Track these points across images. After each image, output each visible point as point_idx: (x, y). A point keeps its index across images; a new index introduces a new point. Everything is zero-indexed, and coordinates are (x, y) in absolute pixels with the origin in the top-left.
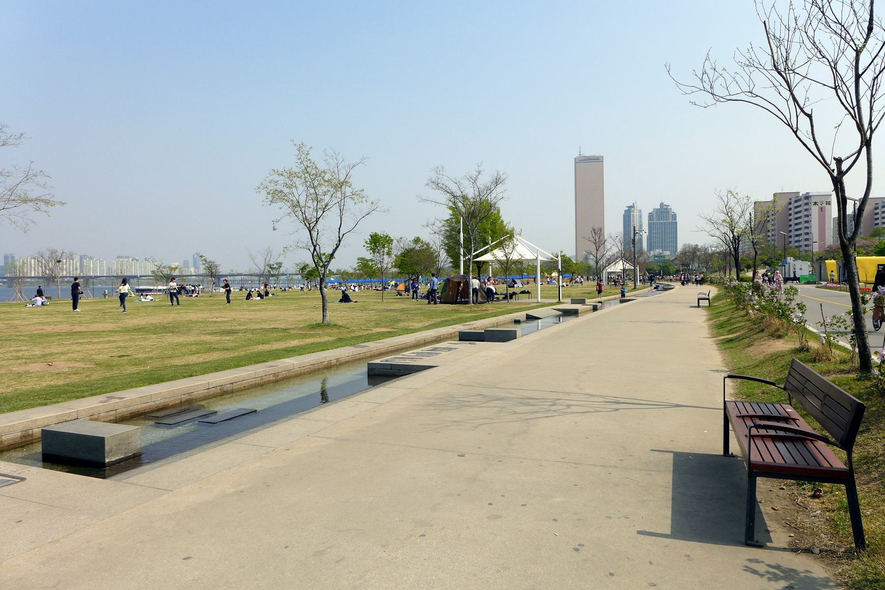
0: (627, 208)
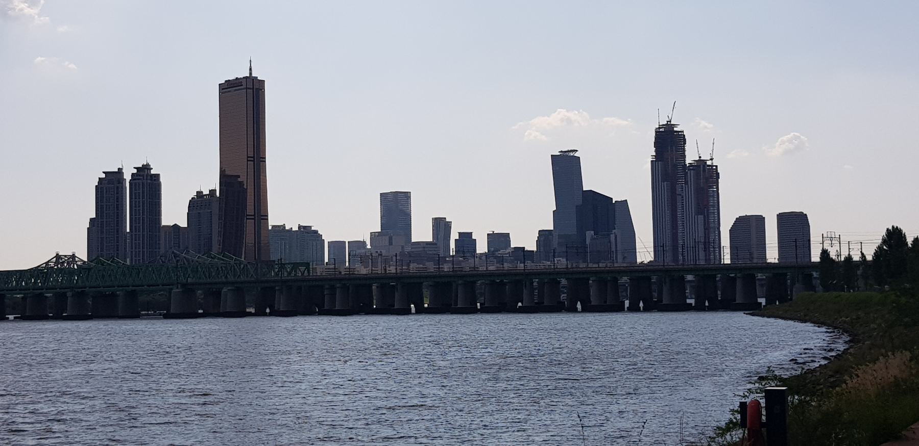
0: (103, 176)
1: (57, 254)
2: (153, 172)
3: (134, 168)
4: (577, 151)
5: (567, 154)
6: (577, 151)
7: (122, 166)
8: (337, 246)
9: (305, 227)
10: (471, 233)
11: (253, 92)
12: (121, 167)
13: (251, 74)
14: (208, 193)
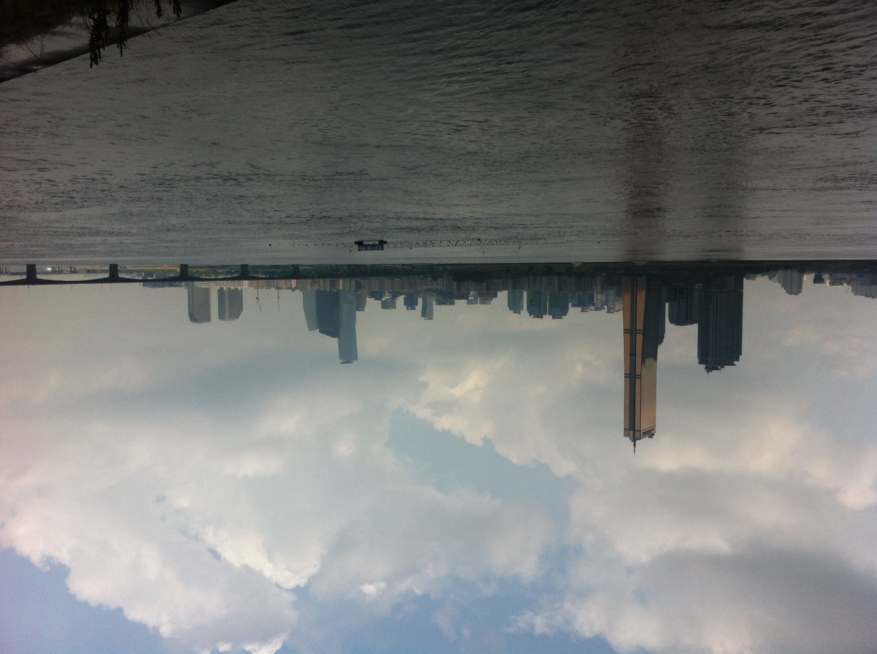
0: (735, 363)
2: (704, 366)
3: (735, 365)
4: (341, 363)
9: (538, 317)
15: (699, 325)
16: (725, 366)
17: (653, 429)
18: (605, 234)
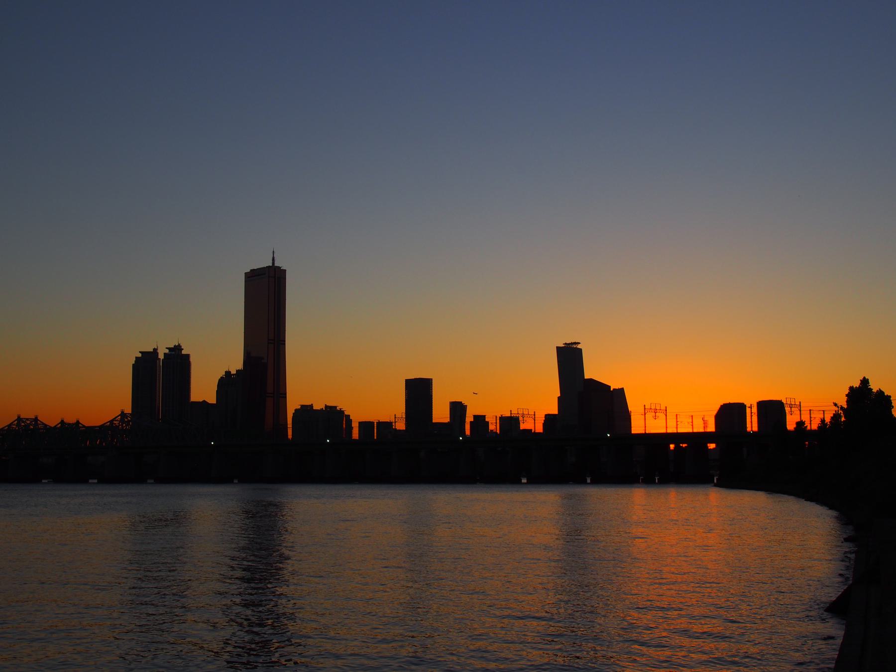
0: (140, 355)
1: (19, 417)
2: (184, 352)
4: (579, 343)
5: (571, 345)
6: (579, 343)
7: (157, 347)
8: (366, 426)
9: (331, 407)
10: (485, 416)
11: (275, 280)
12: (156, 348)
13: (273, 263)
14: (235, 373)
15: (404, 430)
16: (152, 350)
17: (249, 277)
18: (733, 524)
